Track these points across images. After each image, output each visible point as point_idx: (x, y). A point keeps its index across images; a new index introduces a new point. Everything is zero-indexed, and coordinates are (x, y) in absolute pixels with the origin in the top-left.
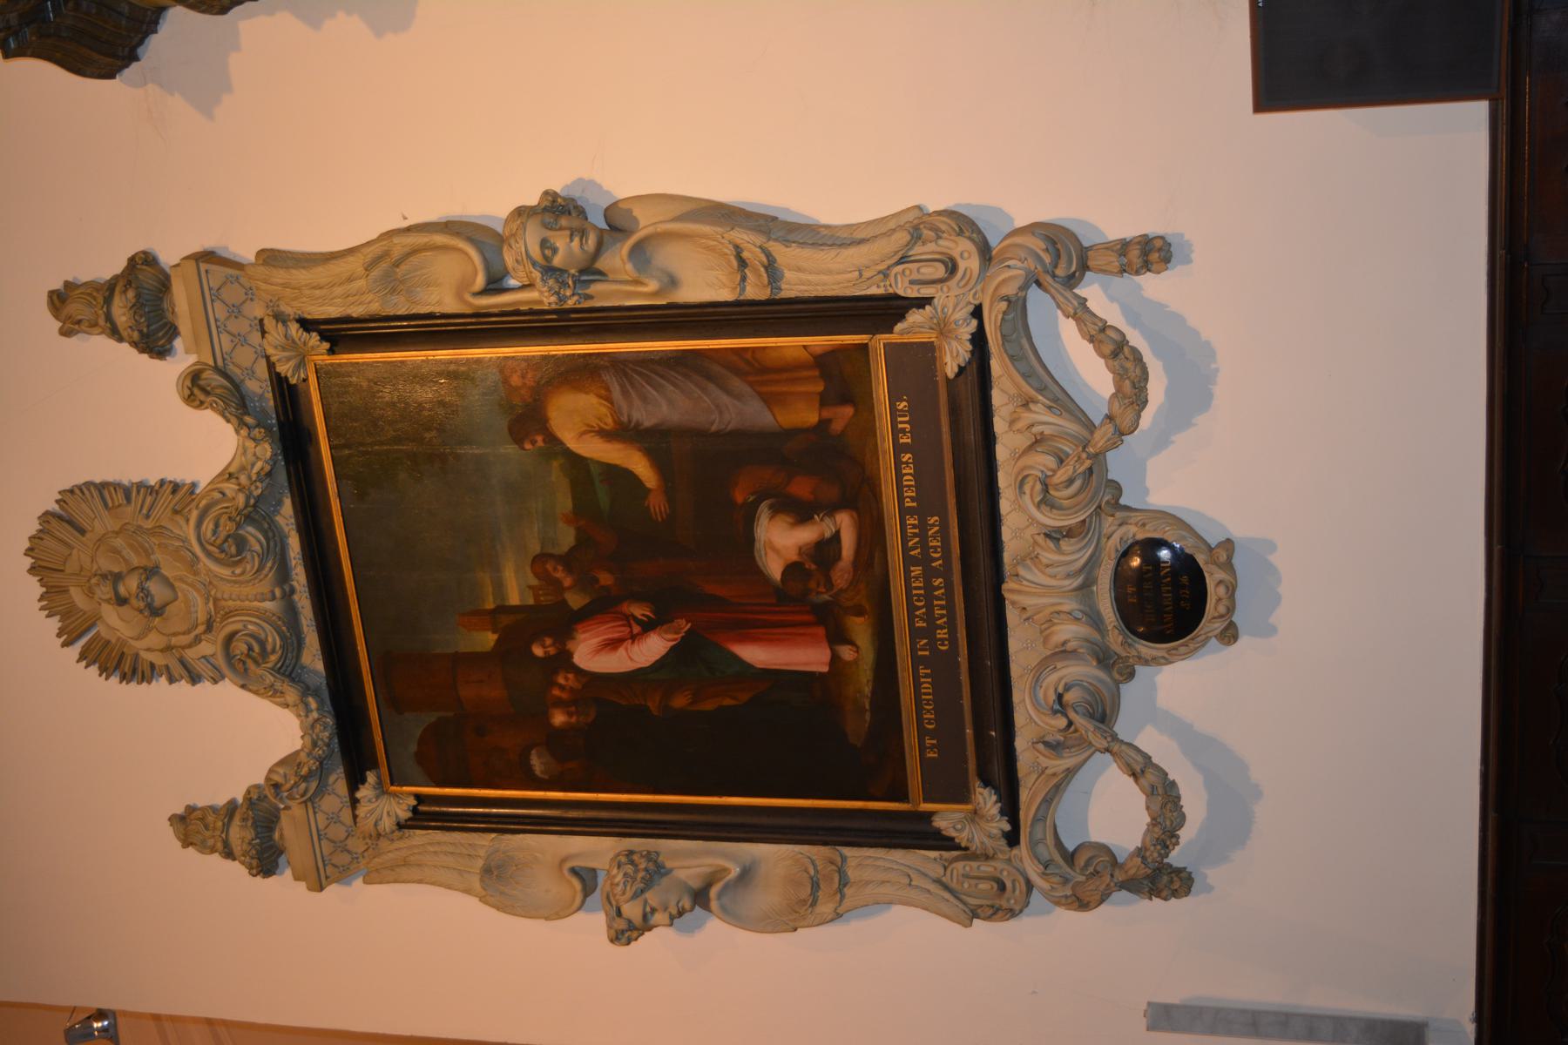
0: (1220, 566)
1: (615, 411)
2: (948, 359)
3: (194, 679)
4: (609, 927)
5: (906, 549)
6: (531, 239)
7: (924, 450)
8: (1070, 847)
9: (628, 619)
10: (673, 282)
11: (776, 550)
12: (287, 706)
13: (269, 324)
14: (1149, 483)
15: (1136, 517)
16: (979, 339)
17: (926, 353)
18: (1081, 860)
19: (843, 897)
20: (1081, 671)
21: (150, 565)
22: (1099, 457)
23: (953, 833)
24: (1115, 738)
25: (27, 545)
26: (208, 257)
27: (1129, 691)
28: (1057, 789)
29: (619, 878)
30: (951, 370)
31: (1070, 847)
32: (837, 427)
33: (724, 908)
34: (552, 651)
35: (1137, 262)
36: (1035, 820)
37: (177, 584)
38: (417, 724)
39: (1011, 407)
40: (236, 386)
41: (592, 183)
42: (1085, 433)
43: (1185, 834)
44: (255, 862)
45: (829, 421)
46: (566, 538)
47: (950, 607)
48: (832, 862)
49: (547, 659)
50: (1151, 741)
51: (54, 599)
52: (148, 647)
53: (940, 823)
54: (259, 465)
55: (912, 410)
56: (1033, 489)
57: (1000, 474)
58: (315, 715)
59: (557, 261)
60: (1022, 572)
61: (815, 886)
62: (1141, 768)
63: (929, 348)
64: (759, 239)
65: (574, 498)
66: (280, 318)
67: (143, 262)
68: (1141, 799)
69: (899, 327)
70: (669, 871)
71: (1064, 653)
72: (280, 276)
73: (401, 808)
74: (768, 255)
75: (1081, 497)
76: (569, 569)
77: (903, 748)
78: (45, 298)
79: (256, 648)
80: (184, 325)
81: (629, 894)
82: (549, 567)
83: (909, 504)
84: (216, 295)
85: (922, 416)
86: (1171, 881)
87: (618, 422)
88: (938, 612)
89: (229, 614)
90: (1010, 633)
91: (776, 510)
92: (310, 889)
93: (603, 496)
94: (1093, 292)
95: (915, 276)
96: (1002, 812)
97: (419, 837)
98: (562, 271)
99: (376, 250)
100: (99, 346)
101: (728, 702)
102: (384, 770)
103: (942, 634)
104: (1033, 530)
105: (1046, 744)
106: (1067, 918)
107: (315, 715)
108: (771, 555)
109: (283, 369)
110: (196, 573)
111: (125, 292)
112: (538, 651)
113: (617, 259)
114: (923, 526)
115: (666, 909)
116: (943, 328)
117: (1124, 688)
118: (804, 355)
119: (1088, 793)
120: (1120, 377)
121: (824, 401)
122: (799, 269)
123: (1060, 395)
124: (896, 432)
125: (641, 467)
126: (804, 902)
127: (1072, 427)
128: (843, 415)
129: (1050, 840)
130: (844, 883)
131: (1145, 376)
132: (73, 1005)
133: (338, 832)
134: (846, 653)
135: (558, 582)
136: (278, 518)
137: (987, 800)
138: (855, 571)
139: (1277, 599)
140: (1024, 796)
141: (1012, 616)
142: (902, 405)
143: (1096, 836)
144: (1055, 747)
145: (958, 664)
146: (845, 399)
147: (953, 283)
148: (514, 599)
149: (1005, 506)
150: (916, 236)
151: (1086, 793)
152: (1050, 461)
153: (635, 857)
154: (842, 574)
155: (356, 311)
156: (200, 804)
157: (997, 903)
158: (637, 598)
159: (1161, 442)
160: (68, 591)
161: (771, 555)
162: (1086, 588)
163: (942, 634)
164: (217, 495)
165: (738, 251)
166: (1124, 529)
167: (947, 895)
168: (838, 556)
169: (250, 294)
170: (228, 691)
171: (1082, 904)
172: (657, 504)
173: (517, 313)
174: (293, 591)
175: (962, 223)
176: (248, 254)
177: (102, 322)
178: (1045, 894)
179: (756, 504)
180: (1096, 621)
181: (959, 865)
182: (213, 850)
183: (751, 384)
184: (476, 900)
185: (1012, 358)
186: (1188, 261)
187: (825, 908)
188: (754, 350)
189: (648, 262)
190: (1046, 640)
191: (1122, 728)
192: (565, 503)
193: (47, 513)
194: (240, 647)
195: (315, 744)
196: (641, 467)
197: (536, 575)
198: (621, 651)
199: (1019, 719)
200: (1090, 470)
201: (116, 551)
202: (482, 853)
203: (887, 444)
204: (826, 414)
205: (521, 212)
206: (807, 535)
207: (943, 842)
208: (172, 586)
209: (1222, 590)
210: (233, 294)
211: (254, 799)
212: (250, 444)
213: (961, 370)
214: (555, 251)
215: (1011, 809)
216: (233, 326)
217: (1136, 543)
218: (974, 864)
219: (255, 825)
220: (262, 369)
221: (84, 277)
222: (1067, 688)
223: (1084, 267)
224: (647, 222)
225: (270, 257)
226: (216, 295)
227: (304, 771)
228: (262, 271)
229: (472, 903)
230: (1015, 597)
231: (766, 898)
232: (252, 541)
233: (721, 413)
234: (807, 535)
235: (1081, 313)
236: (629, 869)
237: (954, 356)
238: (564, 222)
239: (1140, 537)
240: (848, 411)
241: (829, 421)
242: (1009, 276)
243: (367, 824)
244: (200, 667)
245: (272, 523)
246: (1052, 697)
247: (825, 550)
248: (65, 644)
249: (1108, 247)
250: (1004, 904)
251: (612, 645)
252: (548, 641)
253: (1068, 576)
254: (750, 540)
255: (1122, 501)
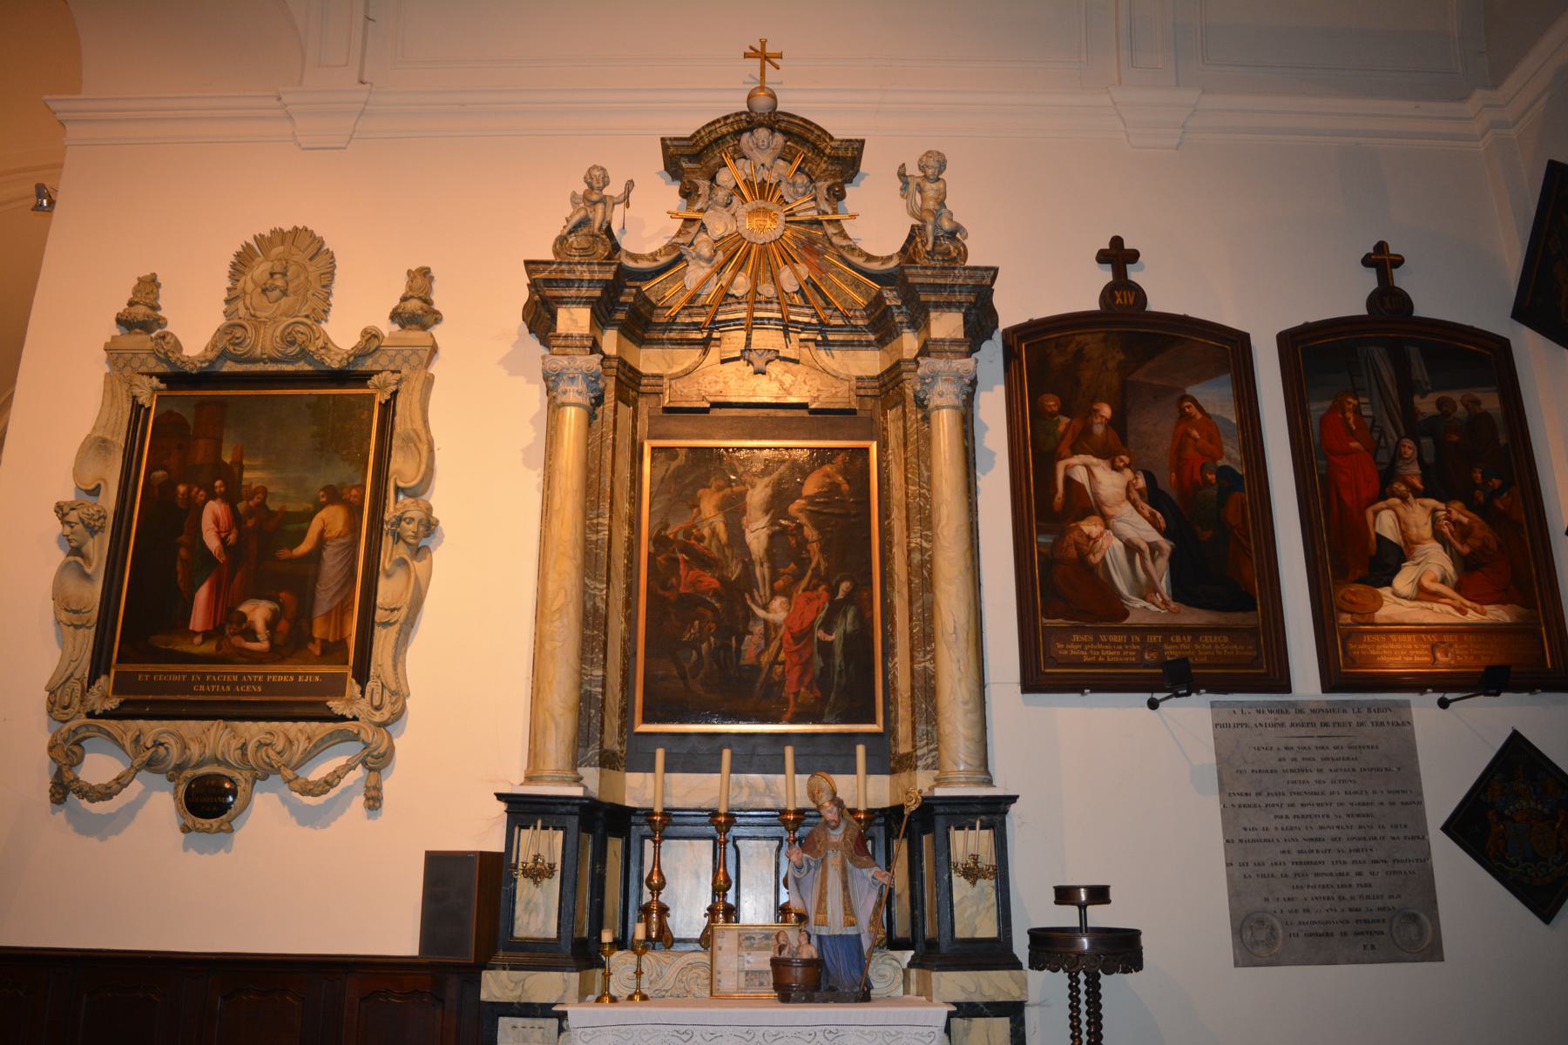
0: (219, 826)
1: (331, 539)
2: (336, 703)
3: (227, 302)
4: (65, 503)
5: (246, 674)
6: (415, 514)
7: (294, 688)
8: (83, 744)
9: (229, 532)
10: (388, 576)
11: (254, 609)
12: (206, 350)
13: (397, 376)
14: (266, 794)
15: (248, 787)
16: (343, 718)
17: (339, 692)
18: (76, 749)
19: (69, 626)
20: (174, 756)
21: (288, 292)
22: (278, 771)
23: (97, 685)
24: (138, 771)
25: (309, 229)
26: (434, 349)
27: (162, 778)
28: (115, 740)
29: (92, 511)
30: (330, 704)
31: (83, 744)
32: (311, 646)
33: (69, 563)
34: (217, 490)
35: (369, 795)
36: (99, 728)
37: (276, 304)
38: (188, 415)
39: (309, 731)
40: (370, 354)
41: (442, 542)
42: (292, 765)
43: (84, 803)
44: (124, 318)
45: (314, 643)
46: (273, 506)
47: (215, 693)
48: (88, 621)
49: (213, 487)
50: (136, 787)
51: (279, 236)
52: (247, 282)
53: (103, 679)
54: (329, 361)
55: (314, 683)
56: (268, 739)
57: (251, 723)
58: (199, 365)
59: (403, 523)
60: (227, 730)
61: (76, 612)
62: (121, 783)
63: (343, 693)
64: (401, 620)
65: (292, 512)
66: (399, 382)
67: (437, 318)
68: (105, 781)
69: (354, 681)
70: (93, 537)
71: (185, 747)
72: (418, 386)
73: (144, 399)
74: (392, 624)
75: (261, 762)
76: (257, 505)
77: (144, 663)
78: (426, 265)
79: (237, 341)
80: (404, 334)
81: (83, 516)
82: (260, 495)
83: (269, 678)
84: (414, 352)
85: (310, 688)
86: (59, 794)
87: (327, 540)
88: (213, 687)
89: (257, 330)
90: (199, 722)
91: (274, 612)
92: (106, 344)
93: (292, 527)
94: (359, 772)
95: (375, 691)
96: (105, 711)
97: (128, 406)
98: (399, 525)
99: (423, 436)
100: (401, 289)
101: (180, 577)
102: (165, 393)
103: (202, 688)
104: (248, 737)
105: (139, 736)
106: (45, 739)
107: (199, 365)
108: (252, 607)
109: (375, 378)
110: (281, 315)
111: (422, 309)
112: (218, 483)
113: (402, 551)
114: (257, 683)
115: (72, 533)
116: (351, 701)
117: (164, 776)
118: (347, 634)
119: (111, 755)
120: (316, 784)
121: (324, 641)
122: (386, 637)
123: (312, 754)
124: (305, 675)
125: (304, 547)
126: (68, 604)
127: (295, 760)
128: (316, 650)
129: (87, 734)
130: (77, 627)
131: (313, 795)
132: (60, 190)
133: (136, 363)
134: (198, 639)
135: (252, 499)
136: (302, 362)
137: (112, 703)
138: (239, 648)
139: (201, 853)
140: (113, 722)
141: (207, 723)
142: (317, 679)
143: (88, 757)
144: (137, 740)
145: (176, 694)
146: (324, 652)
147: (370, 708)
148: (246, 475)
149: (262, 724)
150: (393, 693)
151: (1222, 726)
152: (279, 748)
153: (102, 520)
154: (238, 641)
155: (397, 419)
156: (161, 291)
157: (57, 705)
158: (239, 537)
159: (284, 801)
160: (282, 244)
161: (252, 607)
162: (216, 760)
163: (202, 688)
164: (317, 335)
165: (398, 609)
166: (243, 780)
167: (63, 680)
168: (247, 640)
169: (413, 368)
170: (220, 320)
171: (51, 749)
172: (284, 554)
173: (385, 498)
174: (265, 363)
175: (398, 715)
176: (433, 370)
177: (410, 293)
178: (59, 730)
179: (279, 603)
180: (199, 764)
181: (79, 687)
182: (134, 294)
183: (337, 607)
184: (89, 432)
185: (331, 734)
186: (369, 818)
187: (64, 616)
188: (353, 610)
189: (399, 565)
190: (192, 740)
191: (144, 773)
192: (292, 507)
193: (323, 242)
194: (239, 333)
195: (183, 362)
196: (304, 547)
197: (257, 488)
198: (213, 526)
199: (154, 723)
200: (272, 766)
201: (298, 276)
202: (115, 439)
203: (299, 669)
204: (318, 642)
205: (430, 509)
206: (260, 625)
207: (93, 679)
208: (276, 301)
209: (207, 826)
210: (414, 360)
211: (160, 322)
212: (339, 358)
213: (330, 709)
214: (408, 523)
215: (107, 715)
216: (399, 358)
217: (236, 786)
218: (79, 695)
219: (144, 322)
220: (377, 367)
221: (434, 286)
222: (166, 749)
223: (371, 770)
224: (418, 566)
225: (429, 382)
226: (414, 352)
227: (170, 354)
228: (422, 377)
229: (87, 430)
230: (215, 727)
231: (73, 586)
232: (292, 349)
233: (325, 590)
234: (260, 625)
235: (349, 767)
236: (96, 517)
237: (337, 706)
238: (422, 529)
239: (239, 788)
240: (318, 652)
241: (314, 643)
242: (368, 734)
243: (138, 380)
244: (233, 307)
245: (300, 360)
246: (163, 741)
247: (251, 634)
248: (255, 237)
249: (379, 781)
250: (55, 708)
251: (216, 522)
252: (222, 489)
253: (223, 753)
254: (261, 597)
255: (258, 781)
